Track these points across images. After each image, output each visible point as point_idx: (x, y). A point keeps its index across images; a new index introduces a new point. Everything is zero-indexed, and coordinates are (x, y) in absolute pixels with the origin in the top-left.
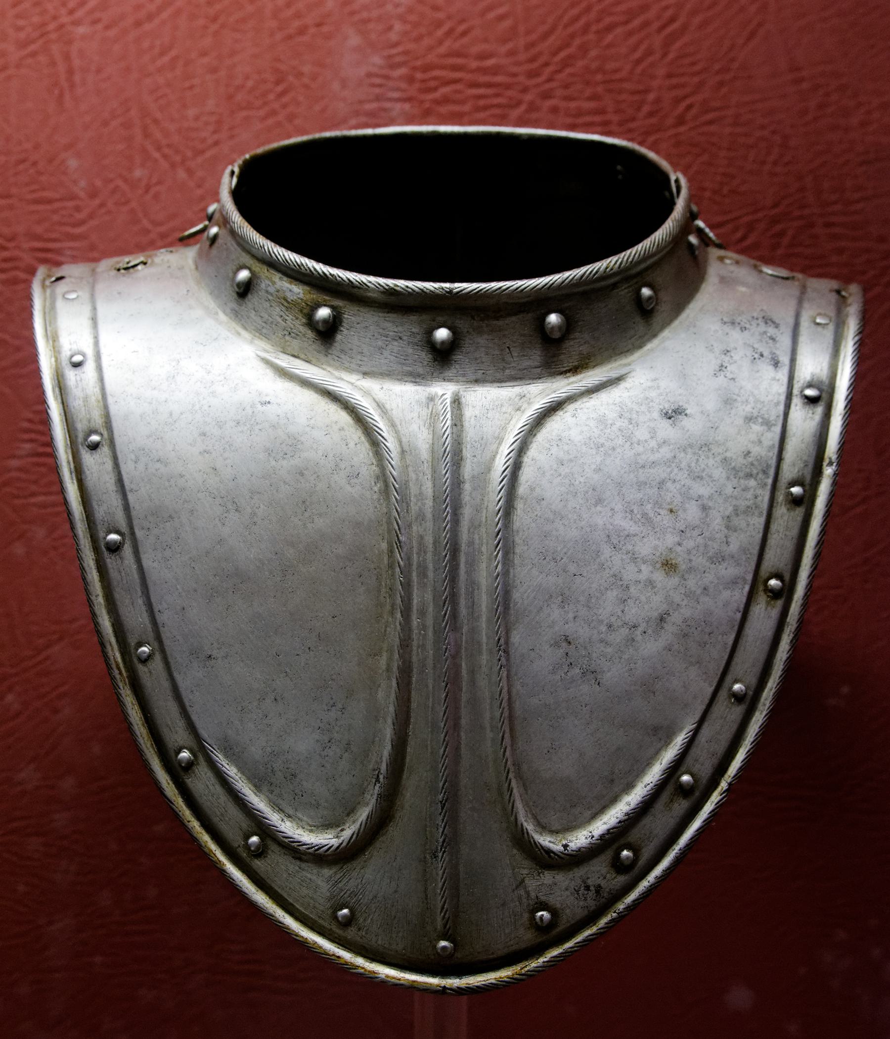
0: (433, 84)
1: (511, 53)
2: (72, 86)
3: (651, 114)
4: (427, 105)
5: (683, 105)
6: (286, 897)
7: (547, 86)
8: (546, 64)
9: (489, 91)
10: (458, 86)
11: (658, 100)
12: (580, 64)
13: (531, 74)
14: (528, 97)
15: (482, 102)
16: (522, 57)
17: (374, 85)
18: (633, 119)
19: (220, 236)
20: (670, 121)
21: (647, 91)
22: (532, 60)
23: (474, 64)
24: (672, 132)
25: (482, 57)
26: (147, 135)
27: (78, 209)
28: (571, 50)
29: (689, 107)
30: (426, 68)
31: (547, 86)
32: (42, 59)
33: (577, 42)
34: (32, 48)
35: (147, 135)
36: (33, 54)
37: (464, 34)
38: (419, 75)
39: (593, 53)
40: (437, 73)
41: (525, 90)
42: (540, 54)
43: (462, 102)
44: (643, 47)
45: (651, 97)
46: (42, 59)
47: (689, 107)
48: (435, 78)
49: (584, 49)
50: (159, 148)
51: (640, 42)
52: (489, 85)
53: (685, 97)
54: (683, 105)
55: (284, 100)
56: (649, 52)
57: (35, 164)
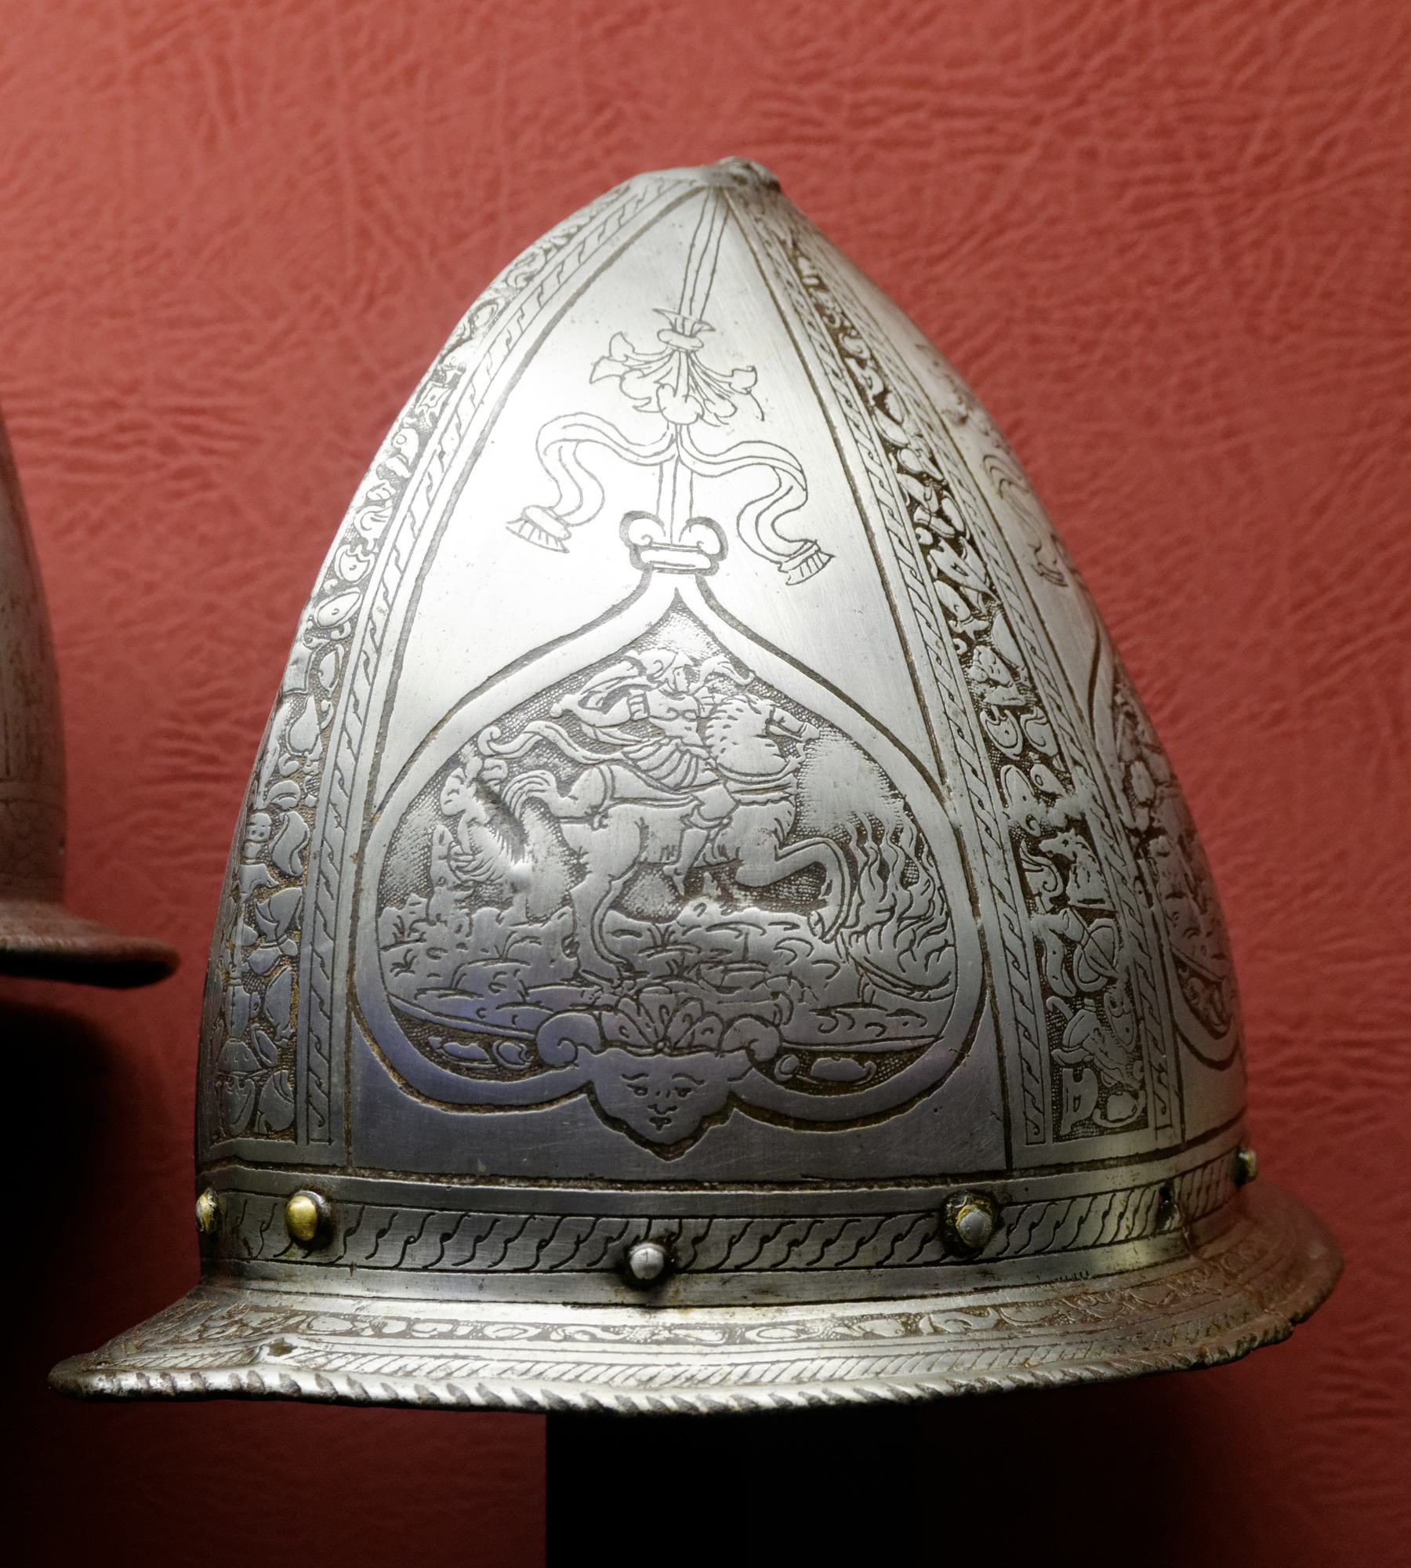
0: (871, 111)
1: (1010, 56)
2: (232, 118)
3: (1260, 160)
4: (132, 400)
5: (1320, 141)
6: (574, 825)
7: (1079, 113)
8: (1074, 74)
9: (973, 124)
10: (76, 432)
11: (1274, 135)
12: (1134, 72)
13: (1051, 92)
14: (1042, 134)
15: (33, 404)
16: (1028, 60)
17: (768, 115)
18: (1231, 169)
19: (181, 972)
20: (1299, 170)
21: (1255, 117)
22: (1045, 68)
23: (943, 76)
24: (1300, 190)
25: (954, 63)
26: (367, 203)
27: (247, 338)
28: (1119, 47)
29: (1328, 147)
30: (859, 84)
31: (1079, 113)
32: (177, 65)
33: (1128, 33)
34: (159, 45)
35: (367, 203)
36: (160, 59)
37: (927, 20)
38: (848, 97)
39: (1157, 53)
40: (882, 92)
41: (1036, 121)
42: (1062, 56)
43: (926, 144)
44: (1243, 44)
45: (1262, 127)
46: (177, 65)
47: (1328, 147)
48: (875, 102)
49: (1140, 46)
50: (389, 229)
51: (1241, 30)
52: (970, 113)
53: (1326, 126)
54: (1320, 141)
55: (613, 139)
56: (1256, 48)
57: (169, 254)
